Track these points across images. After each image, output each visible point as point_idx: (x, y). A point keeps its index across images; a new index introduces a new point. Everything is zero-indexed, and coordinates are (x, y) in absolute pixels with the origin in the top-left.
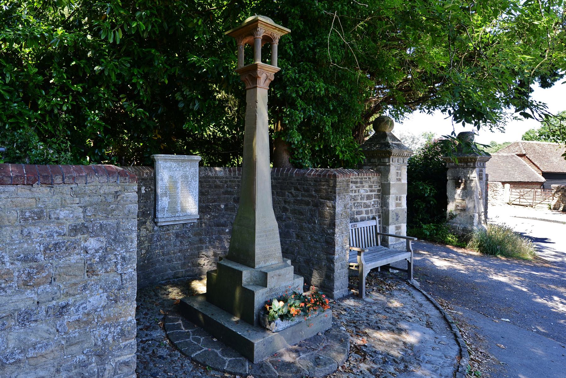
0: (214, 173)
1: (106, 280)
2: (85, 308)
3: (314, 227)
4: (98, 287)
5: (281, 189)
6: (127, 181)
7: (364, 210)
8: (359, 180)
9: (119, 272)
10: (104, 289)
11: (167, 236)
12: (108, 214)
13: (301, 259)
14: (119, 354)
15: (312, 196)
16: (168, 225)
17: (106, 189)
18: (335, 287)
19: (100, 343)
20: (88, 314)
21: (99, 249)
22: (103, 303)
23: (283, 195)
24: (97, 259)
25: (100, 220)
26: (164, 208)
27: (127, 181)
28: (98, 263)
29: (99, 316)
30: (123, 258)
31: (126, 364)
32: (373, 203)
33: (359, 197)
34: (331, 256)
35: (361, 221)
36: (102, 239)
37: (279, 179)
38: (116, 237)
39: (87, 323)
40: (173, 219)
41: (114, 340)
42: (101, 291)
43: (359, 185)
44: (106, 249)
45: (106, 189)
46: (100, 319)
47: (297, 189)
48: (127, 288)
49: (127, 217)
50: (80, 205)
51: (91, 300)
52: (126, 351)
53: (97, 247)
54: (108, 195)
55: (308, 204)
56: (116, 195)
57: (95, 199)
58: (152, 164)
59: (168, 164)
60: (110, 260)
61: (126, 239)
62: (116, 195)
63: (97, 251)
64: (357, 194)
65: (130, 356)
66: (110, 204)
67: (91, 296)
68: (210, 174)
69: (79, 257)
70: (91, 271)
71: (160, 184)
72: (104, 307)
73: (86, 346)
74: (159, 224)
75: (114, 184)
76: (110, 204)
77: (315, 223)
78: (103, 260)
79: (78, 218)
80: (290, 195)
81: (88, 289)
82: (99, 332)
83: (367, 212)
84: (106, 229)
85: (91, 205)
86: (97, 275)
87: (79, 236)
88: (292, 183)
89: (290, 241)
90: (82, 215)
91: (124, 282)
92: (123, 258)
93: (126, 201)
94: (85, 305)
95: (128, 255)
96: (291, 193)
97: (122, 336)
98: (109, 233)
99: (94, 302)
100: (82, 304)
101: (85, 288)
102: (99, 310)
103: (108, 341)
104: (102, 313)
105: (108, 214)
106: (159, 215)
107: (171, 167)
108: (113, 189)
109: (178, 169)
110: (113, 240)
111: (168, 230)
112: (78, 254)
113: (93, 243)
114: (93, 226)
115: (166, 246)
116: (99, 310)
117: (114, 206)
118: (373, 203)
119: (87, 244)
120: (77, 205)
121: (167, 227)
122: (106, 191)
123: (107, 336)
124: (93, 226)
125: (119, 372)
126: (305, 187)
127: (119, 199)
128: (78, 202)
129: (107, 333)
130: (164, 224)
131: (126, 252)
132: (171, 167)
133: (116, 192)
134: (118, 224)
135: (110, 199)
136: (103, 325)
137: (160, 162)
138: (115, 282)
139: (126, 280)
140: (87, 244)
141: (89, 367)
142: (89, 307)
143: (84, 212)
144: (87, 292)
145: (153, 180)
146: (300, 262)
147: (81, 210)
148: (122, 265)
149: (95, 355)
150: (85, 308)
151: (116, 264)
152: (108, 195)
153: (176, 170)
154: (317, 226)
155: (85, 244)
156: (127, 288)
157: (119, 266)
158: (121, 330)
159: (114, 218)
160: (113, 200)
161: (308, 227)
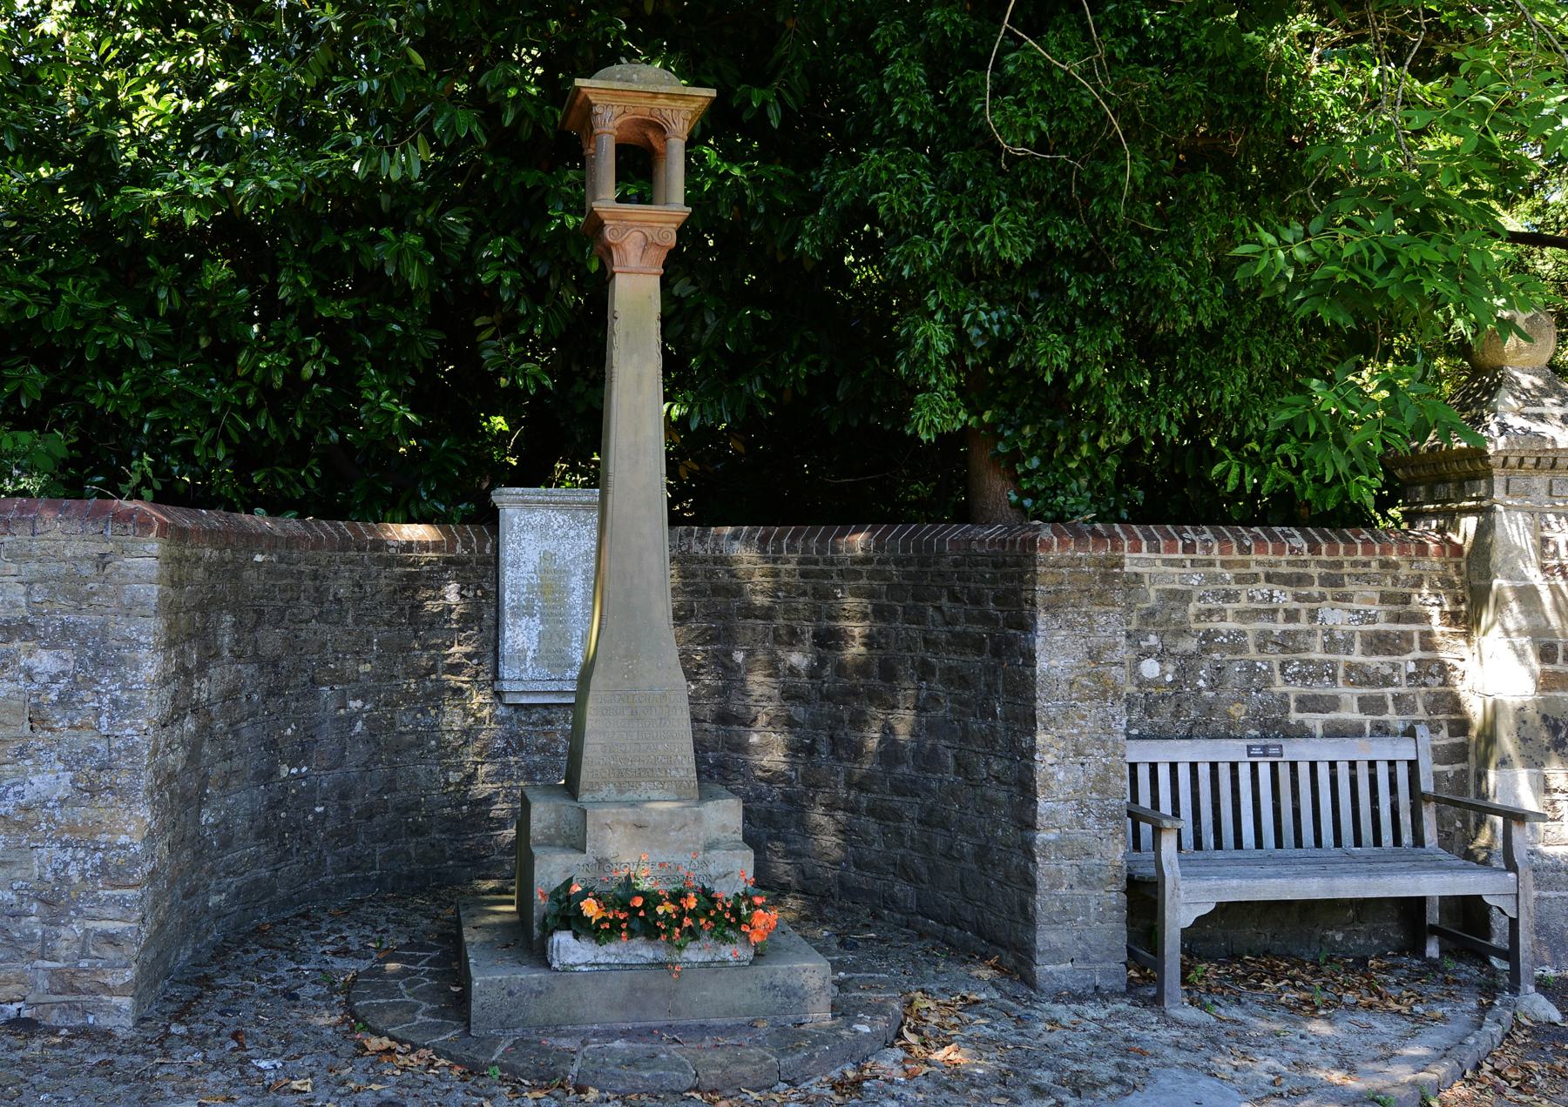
0: (710, 544)
1: (71, 745)
2: (19, 794)
3: (993, 729)
4: (54, 756)
5: (914, 597)
6: (131, 531)
7: (1349, 694)
8: (1314, 571)
9: (103, 731)
10: (66, 762)
11: (543, 740)
12: (81, 600)
13: (967, 848)
14: (93, 911)
15: (987, 619)
16: (546, 706)
17: (76, 547)
18: (1040, 945)
19: (49, 876)
20: (27, 809)
21: (57, 676)
22: (61, 793)
23: (920, 618)
24: (53, 697)
25: (63, 612)
26: (523, 651)
27: (131, 531)
28: (54, 704)
29: (50, 819)
30: (115, 702)
31: (111, 939)
32: (1412, 668)
33: (1318, 642)
34: (1028, 834)
35: (1327, 735)
36: (65, 654)
37: (910, 561)
38: (97, 654)
39: (22, 826)
40: (553, 687)
41: (84, 879)
42: (60, 766)
43: (1315, 590)
44: (74, 676)
45: (76, 547)
46: (52, 825)
47: (954, 597)
48: (120, 769)
49: (128, 611)
50: (21, 578)
51: (34, 780)
52: (110, 910)
53: (55, 671)
54: (82, 560)
55: (978, 645)
56: (102, 561)
57: (53, 568)
58: (489, 518)
59: (538, 517)
60: (82, 702)
61: (122, 660)
62: (102, 561)
63: (54, 679)
64: (1303, 625)
65: (122, 925)
66: (86, 580)
67: (37, 772)
68: (696, 548)
69: (13, 685)
70: (37, 720)
71: (509, 576)
72: (63, 802)
73: (18, 874)
74: (508, 699)
75: (96, 537)
76: (86, 580)
77: (994, 715)
78: (64, 701)
79: (14, 605)
80: (938, 617)
81: (30, 757)
82: (50, 853)
83: (1365, 705)
84: (74, 634)
85: (44, 580)
86: (51, 729)
87: (17, 644)
88: (941, 575)
89: (940, 781)
90: (23, 601)
91: (115, 755)
92: (115, 702)
93: (125, 575)
94: (20, 788)
95: (126, 696)
96: (939, 609)
97: (103, 874)
98: (83, 643)
99: (42, 787)
100: (13, 785)
101: (22, 753)
102: (50, 804)
103: (68, 877)
104: (57, 812)
105: (81, 600)
106: (506, 672)
107: (547, 526)
108: (95, 549)
109: (572, 533)
110: (92, 660)
111: (549, 722)
112: (11, 680)
113: (45, 661)
114: (47, 625)
115: (543, 769)
116: (50, 804)
117: (96, 585)
118: (1412, 668)
119: (33, 661)
120: (14, 579)
121: (545, 713)
122: (78, 552)
123: (66, 864)
124: (47, 625)
125: (93, 953)
126: (972, 585)
127: (107, 571)
128: (14, 572)
129: (68, 859)
130: (524, 700)
131: (123, 689)
132: (547, 526)
133: (103, 556)
134: (104, 625)
135: (87, 569)
136: (59, 839)
137: (509, 511)
138: (91, 752)
139: (118, 751)
140: (33, 661)
141: (24, 921)
142: (29, 795)
143: (28, 594)
144: (28, 762)
145: (492, 564)
146: (963, 857)
147: (22, 589)
148: (111, 717)
149: (36, 898)
150: (19, 794)
151: (98, 712)
152: (82, 560)
153: (566, 535)
154: (1000, 725)
155: (29, 662)
156: (120, 769)
157: (103, 719)
158: (103, 861)
159: (95, 612)
160: (94, 571)
161: (980, 729)
